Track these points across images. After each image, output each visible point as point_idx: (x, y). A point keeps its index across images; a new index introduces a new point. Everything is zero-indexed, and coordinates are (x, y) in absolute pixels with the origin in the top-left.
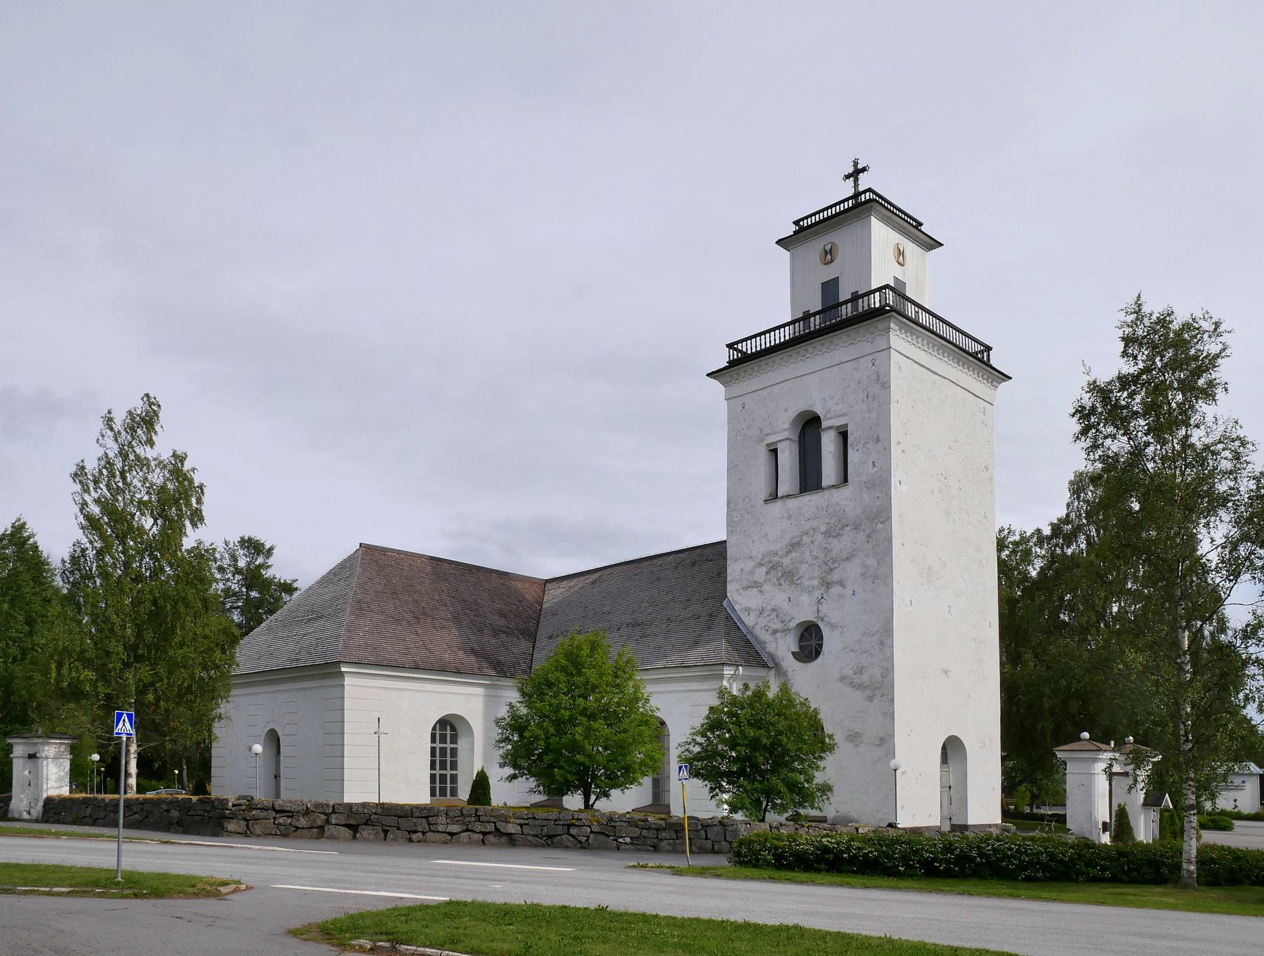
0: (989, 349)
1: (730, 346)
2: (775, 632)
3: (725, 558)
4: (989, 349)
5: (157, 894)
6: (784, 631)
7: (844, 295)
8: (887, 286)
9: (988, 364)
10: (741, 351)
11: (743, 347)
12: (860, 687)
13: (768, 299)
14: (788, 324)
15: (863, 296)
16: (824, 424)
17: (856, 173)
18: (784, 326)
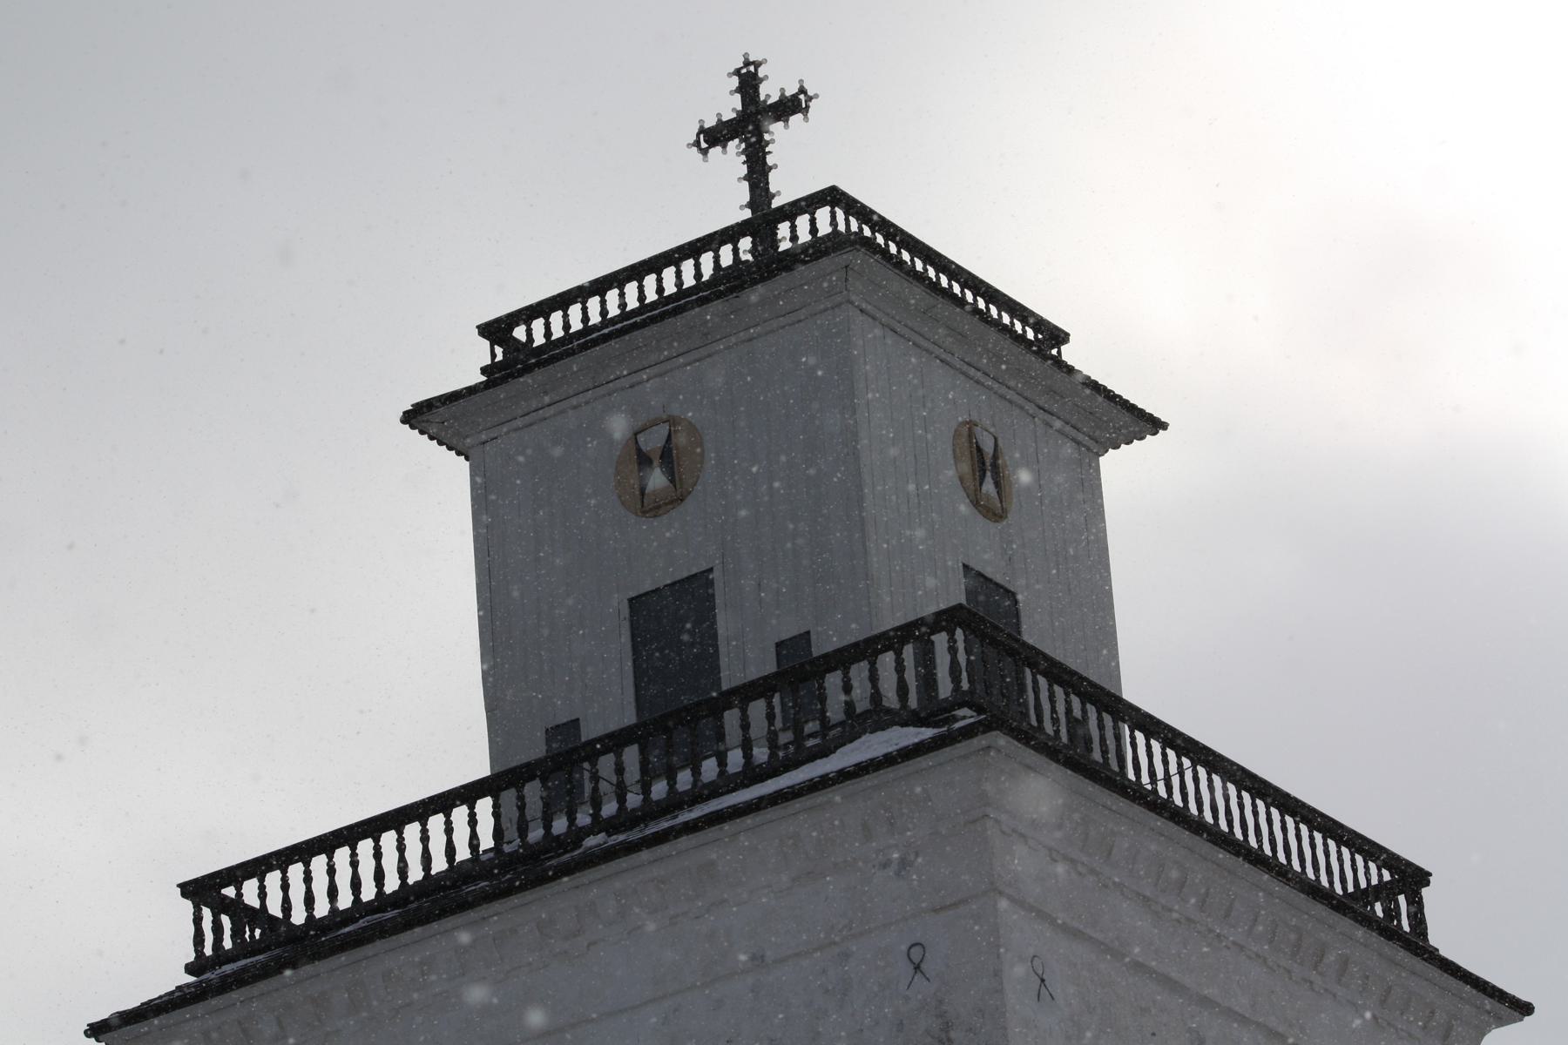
1: (200, 891)
4: (1411, 879)
5: (1491, 996)
7: (744, 654)
9: (1416, 942)
10: (259, 916)
14: (468, 794)
15: (843, 658)
17: (752, 120)
18: (443, 803)
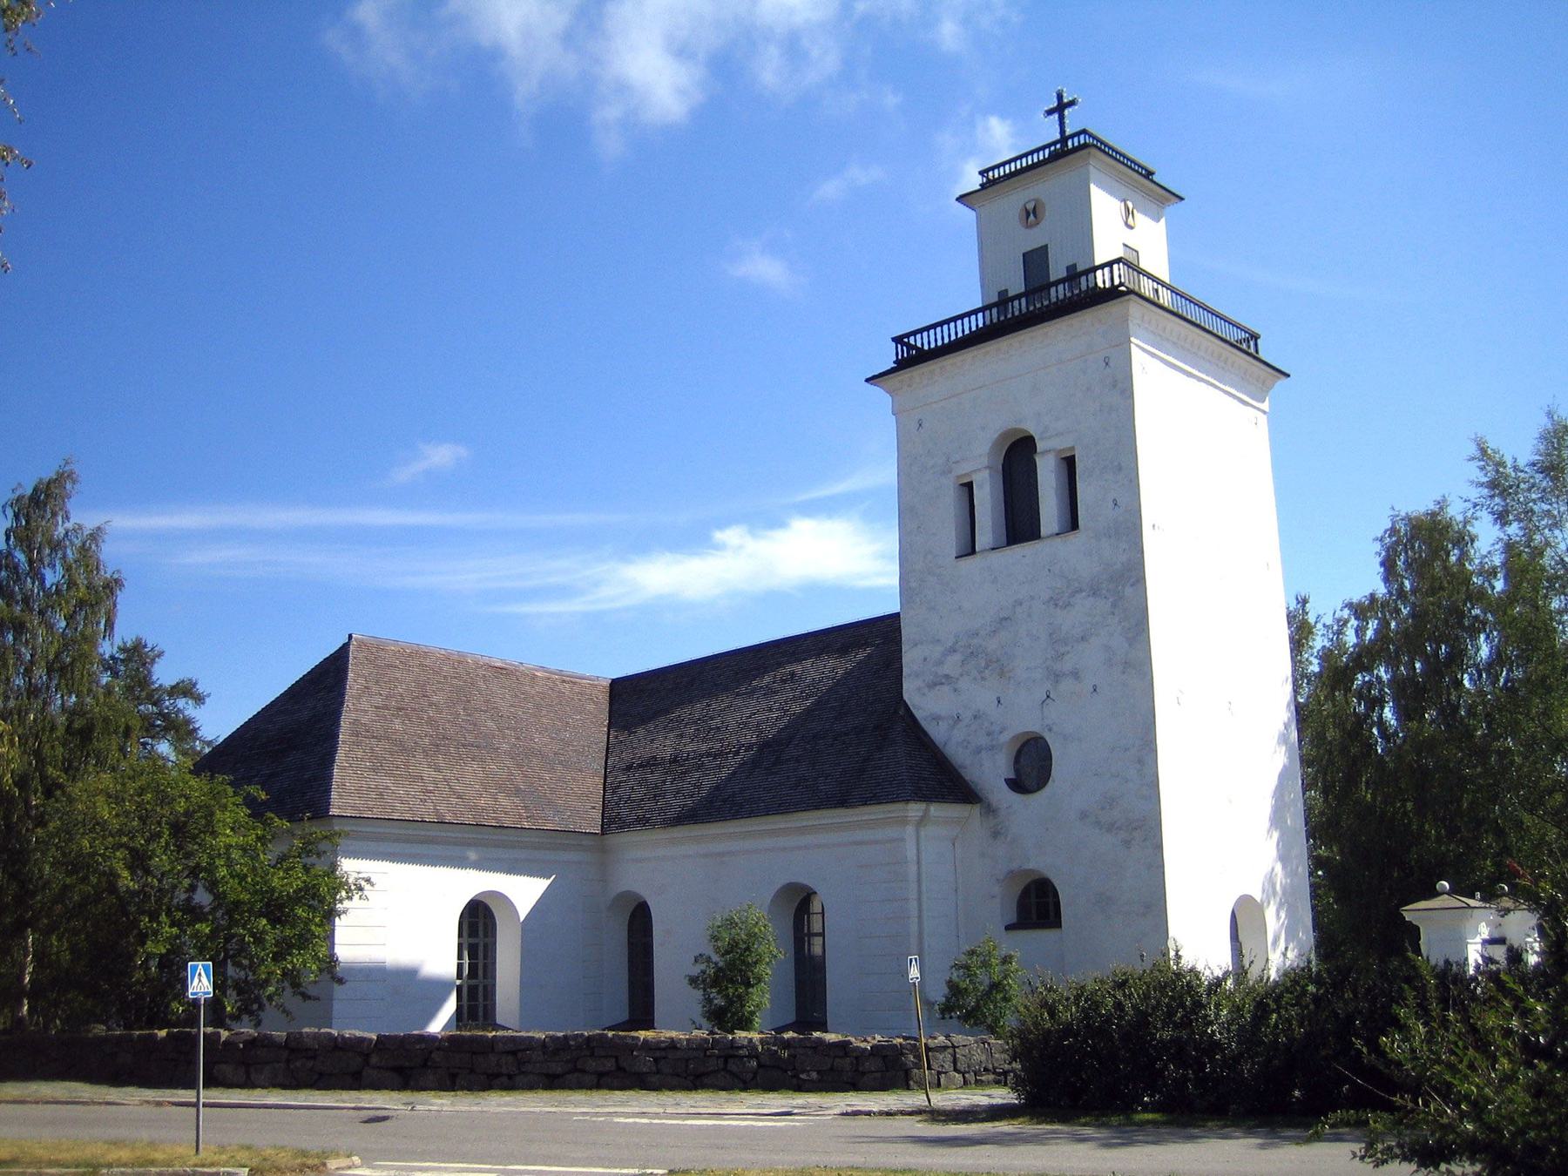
0: (1255, 337)
1: (898, 340)
2: (978, 750)
3: (898, 642)
6: (992, 748)
7: (1057, 271)
8: (1118, 261)
10: (915, 347)
11: (916, 341)
12: (1111, 828)
13: (952, 280)
16: (1040, 446)
17: (1061, 108)
